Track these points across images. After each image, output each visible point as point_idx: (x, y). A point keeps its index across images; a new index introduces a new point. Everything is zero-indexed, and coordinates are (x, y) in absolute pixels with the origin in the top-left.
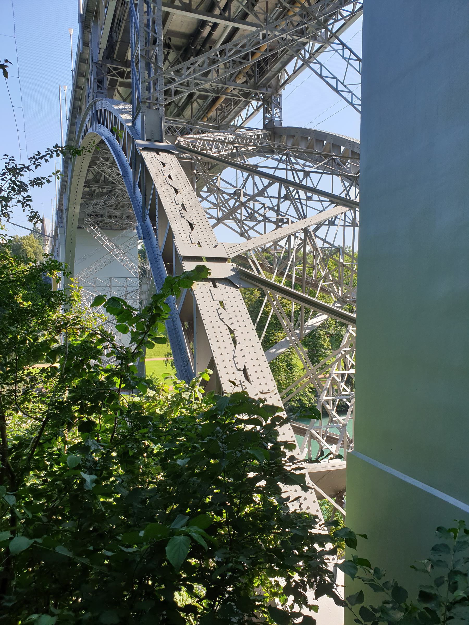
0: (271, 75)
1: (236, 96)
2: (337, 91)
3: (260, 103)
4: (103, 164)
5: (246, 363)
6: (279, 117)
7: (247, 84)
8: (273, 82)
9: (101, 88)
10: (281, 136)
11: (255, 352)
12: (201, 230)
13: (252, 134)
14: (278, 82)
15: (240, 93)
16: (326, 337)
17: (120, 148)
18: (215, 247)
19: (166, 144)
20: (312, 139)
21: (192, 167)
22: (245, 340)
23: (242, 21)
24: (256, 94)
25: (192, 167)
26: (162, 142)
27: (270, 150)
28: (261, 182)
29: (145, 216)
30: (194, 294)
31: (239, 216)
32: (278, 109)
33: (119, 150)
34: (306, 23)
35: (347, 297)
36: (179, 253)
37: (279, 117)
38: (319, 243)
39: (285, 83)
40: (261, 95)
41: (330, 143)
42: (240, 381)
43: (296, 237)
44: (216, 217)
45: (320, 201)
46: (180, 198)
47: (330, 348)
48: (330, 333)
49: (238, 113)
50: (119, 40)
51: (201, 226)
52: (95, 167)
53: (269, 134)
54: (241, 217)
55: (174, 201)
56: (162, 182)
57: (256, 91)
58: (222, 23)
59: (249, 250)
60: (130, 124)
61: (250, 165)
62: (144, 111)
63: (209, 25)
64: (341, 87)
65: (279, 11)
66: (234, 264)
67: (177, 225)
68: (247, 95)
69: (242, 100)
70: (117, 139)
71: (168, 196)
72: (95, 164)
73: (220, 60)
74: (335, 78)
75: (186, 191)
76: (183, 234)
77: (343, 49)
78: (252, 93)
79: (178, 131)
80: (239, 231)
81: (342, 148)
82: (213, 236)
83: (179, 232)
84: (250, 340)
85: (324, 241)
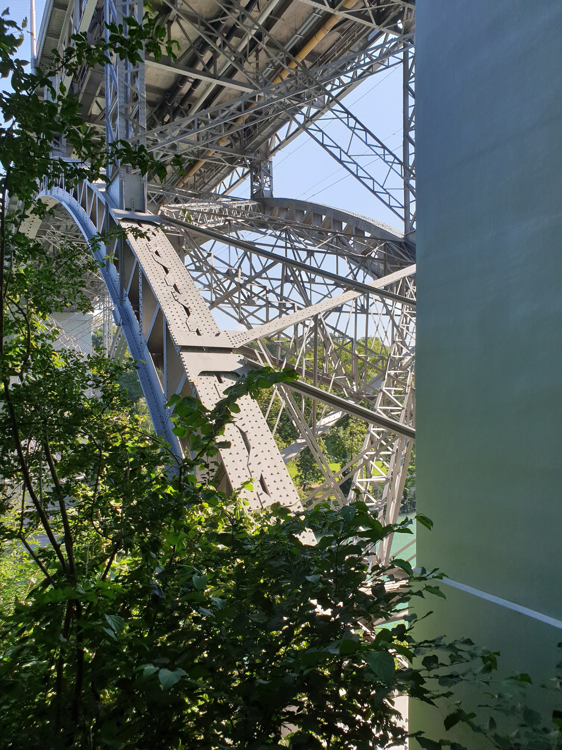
0: (260, 140)
1: (219, 160)
2: (340, 161)
3: (246, 170)
4: (54, 233)
5: (263, 471)
6: (269, 186)
7: (232, 147)
8: (262, 147)
9: (58, 144)
10: (272, 208)
11: (272, 458)
12: (199, 316)
13: (240, 205)
14: (268, 147)
15: (224, 157)
16: (321, 440)
17: (87, 216)
18: (218, 335)
19: (148, 215)
20: (308, 213)
21: (179, 242)
22: (259, 444)
23: (188, 68)
24: (243, 159)
25: (179, 242)
26: (144, 212)
27: (259, 224)
28: (258, 262)
29: (122, 297)
30: (196, 390)
31: (237, 301)
32: (268, 178)
33: (85, 219)
34: (307, 88)
35: (362, 394)
36: (176, 343)
37: (269, 186)
38: (329, 331)
39: (276, 149)
40: (248, 161)
41: (330, 218)
42: (257, 493)
43: (305, 326)
44: (210, 300)
45: (325, 284)
46: (171, 278)
47: (327, 452)
48: (325, 434)
49: (220, 180)
50: (83, 91)
51: (199, 311)
52: (43, 236)
53: (259, 205)
54: (239, 301)
55: (164, 282)
56: (148, 259)
57: (243, 156)
58: (205, 79)
59: (256, 339)
60: (104, 190)
61: (246, 242)
62: (122, 175)
63: (189, 81)
64: (344, 158)
65: (270, 72)
66: (240, 355)
67: (170, 310)
68: (232, 160)
69: (225, 166)
70: (83, 205)
71: (157, 276)
72: (45, 233)
73: (210, 122)
74: (338, 147)
75: (177, 270)
76: (178, 321)
77: (348, 118)
78: (238, 158)
79: (153, 199)
80: (237, 317)
81: (344, 225)
82: (213, 322)
83: (174, 318)
84: (266, 443)
85: (335, 329)
